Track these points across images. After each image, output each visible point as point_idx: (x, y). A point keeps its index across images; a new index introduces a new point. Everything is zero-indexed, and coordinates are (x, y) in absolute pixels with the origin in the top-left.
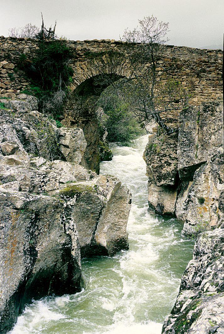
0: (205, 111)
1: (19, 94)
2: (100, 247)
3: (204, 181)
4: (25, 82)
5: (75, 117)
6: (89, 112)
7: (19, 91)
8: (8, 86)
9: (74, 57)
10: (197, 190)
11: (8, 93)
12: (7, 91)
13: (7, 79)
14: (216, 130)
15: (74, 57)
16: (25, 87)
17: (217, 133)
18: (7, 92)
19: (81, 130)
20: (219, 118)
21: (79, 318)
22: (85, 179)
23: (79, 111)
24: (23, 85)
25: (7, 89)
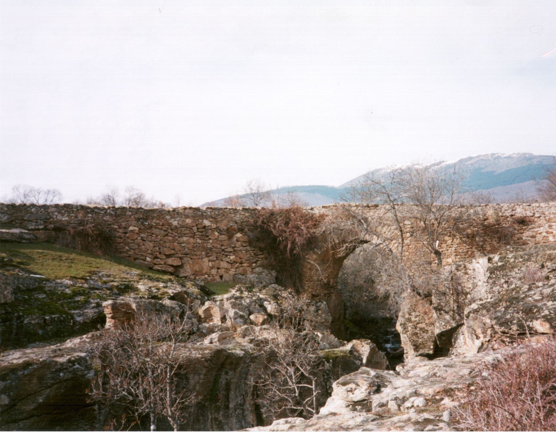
0: (457, 270)
1: (255, 268)
2: (25, 345)
3: (463, 343)
4: (260, 255)
5: (316, 290)
6: (331, 283)
7: (254, 265)
8: (243, 260)
9: (190, 372)
10: (457, 353)
11: (243, 268)
12: (243, 265)
13: (242, 253)
14: (471, 289)
15: (190, 372)
16: (261, 259)
17: (473, 292)
18: (242, 266)
19: (325, 303)
20: (473, 277)
21: (74, 303)
22: (499, 320)
23: (319, 283)
24: (259, 258)
25: (241, 263)
